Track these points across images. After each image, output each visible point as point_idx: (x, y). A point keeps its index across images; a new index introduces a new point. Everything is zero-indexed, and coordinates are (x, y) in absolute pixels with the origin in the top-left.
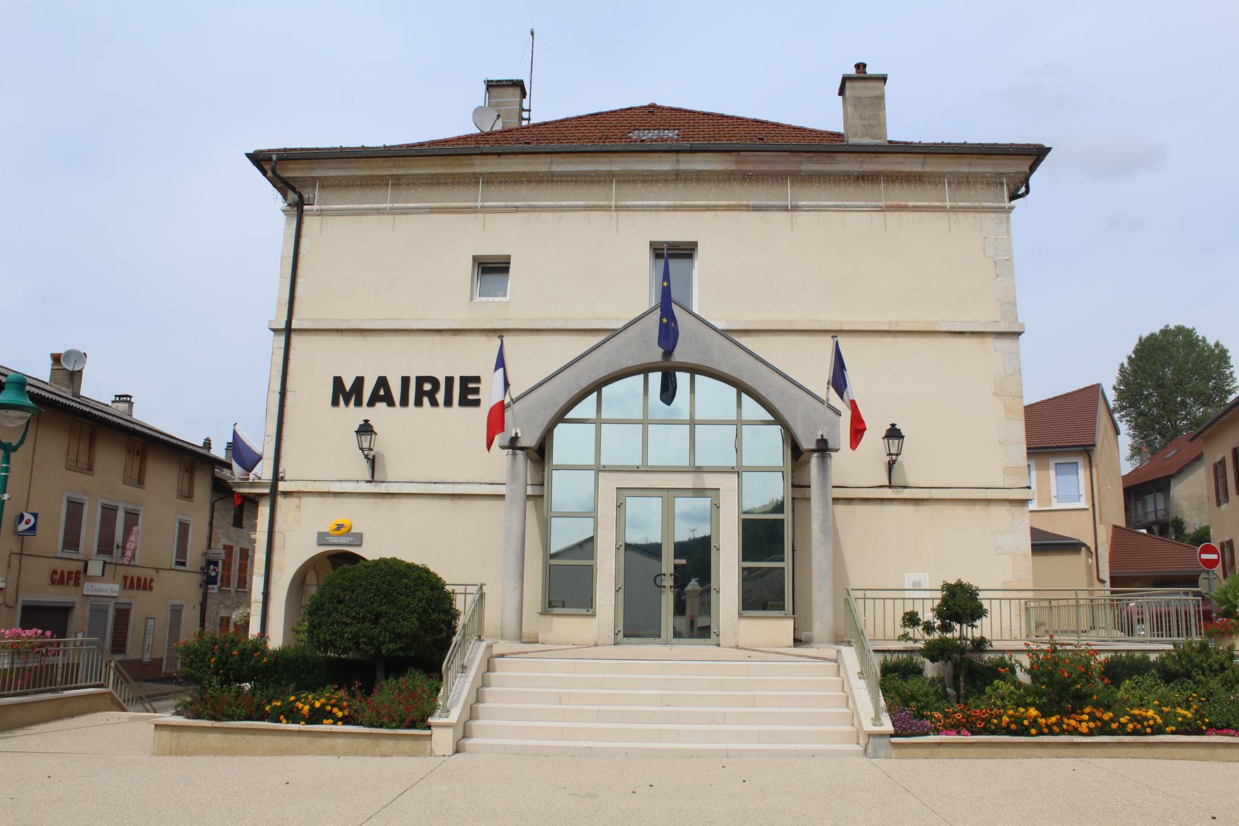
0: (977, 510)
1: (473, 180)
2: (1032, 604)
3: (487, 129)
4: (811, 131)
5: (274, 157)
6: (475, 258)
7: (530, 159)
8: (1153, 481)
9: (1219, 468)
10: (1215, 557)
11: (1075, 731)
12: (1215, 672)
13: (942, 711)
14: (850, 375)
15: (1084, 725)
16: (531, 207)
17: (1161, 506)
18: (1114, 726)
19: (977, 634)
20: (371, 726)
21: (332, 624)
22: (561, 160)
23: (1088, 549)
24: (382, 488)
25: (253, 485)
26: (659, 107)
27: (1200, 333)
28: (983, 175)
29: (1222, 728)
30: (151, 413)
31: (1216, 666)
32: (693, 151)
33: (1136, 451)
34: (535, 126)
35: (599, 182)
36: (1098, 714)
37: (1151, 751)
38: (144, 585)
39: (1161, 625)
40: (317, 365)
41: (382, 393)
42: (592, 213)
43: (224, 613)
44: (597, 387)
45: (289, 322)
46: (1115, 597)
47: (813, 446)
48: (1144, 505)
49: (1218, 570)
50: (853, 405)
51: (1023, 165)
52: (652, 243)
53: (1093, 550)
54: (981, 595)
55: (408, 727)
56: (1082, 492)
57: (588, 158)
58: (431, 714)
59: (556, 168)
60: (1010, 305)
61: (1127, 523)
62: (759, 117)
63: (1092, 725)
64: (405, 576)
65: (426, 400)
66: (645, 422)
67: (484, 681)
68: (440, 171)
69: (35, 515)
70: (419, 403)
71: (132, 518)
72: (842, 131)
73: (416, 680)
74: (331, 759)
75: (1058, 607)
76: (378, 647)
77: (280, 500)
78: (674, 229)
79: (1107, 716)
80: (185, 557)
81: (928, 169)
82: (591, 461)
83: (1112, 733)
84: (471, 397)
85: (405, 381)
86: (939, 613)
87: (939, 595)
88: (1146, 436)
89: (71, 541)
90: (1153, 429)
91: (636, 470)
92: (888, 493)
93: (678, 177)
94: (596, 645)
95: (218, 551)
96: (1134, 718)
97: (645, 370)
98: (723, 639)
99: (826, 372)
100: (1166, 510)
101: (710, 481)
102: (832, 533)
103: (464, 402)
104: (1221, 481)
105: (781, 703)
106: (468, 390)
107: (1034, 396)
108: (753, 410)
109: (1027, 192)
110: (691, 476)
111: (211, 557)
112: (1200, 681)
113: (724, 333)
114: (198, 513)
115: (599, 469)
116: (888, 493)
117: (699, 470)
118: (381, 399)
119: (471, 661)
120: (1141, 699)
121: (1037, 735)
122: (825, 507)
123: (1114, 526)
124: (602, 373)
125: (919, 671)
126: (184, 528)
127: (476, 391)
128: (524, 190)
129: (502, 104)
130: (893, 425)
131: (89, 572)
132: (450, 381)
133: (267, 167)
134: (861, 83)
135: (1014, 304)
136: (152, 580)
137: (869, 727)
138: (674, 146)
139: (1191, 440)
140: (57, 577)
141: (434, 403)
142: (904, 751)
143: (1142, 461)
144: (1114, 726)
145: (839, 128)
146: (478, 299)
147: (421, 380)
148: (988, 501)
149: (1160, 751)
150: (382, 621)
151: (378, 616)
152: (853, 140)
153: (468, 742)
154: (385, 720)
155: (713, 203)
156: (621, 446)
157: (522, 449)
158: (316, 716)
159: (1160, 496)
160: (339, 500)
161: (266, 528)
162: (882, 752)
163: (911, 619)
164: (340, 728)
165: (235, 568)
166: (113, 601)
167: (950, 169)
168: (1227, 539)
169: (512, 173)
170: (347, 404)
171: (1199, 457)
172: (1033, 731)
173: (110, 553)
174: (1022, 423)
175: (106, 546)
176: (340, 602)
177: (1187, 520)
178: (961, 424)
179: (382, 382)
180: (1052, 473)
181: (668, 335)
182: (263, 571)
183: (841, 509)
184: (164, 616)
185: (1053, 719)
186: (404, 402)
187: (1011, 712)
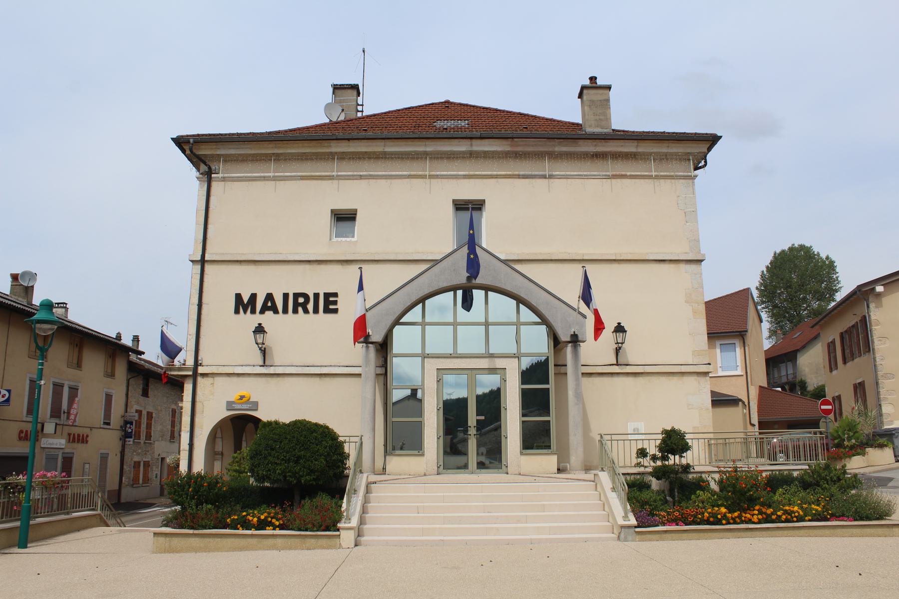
0: (675, 380)
1: (331, 157)
2: (713, 442)
3: (334, 120)
4: (558, 121)
5: (191, 141)
6: (332, 211)
7: (370, 143)
8: (785, 354)
9: (831, 346)
10: (830, 407)
11: (750, 521)
12: (835, 482)
13: (666, 511)
14: (594, 292)
15: (755, 517)
16: (371, 175)
17: (790, 371)
18: (774, 517)
19: (684, 461)
20: (300, 530)
21: (268, 464)
22: (391, 143)
23: (743, 403)
24: (271, 370)
25: (180, 369)
26: (452, 103)
27: (816, 250)
28: (676, 154)
29: (840, 516)
30: (81, 315)
31: (835, 478)
32: (481, 138)
33: (773, 333)
34: (368, 117)
35: (417, 158)
36: (764, 510)
37: (797, 532)
38: (82, 439)
39: (797, 453)
40: (224, 285)
41: (269, 304)
42: (413, 180)
43: (136, 459)
44: (422, 300)
45: (203, 255)
46: (762, 436)
47: (569, 339)
48: (779, 371)
49: (832, 416)
50: (596, 312)
51: (703, 148)
52: (454, 201)
53: (746, 403)
54: (687, 436)
55: (324, 530)
56: (739, 364)
57: (410, 142)
58: (339, 521)
59: (388, 149)
60: (695, 242)
61: (768, 383)
62: (522, 112)
63: (760, 517)
64: (315, 431)
65: (300, 309)
66: (455, 324)
67: (366, 501)
68: (308, 150)
69: (9, 391)
70: (295, 311)
71: (74, 391)
72: (580, 122)
73: (323, 499)
74: (275, 552)
75: (729, 443)
76: (288, 479)
77: (199, 379)
78: (469, 191)
79: (770, 511)
80: (110, 419)
81: (640, 150)
82: (419, 351)
83: (773, 522)
84: (331, 307)
85: (286, 296)
86: (661, 449)
87: (660, 437)
88: (779, 322)
89: (32, 408)
90: (785, 317)
91: (450, 356)
92: (616, 369)
93: (472, 155)
94: (425, 475)
95: (133, 414)
96: (786, 512)
97: (454, 289)
98: (510, 470)
99: (578, 289)
100: (795, 374)
101: (499, 363)
102: (579, 396)
103: (327, 310)
104: (832, 355)
105: (551, 511)
106: (330, 303)
107: (707, 300)
108: (526, 314)
109: (705, 165)
110: (487, 360)
111: (128, 419)
112: (825, 488)
113: (505, 262)
114: (118, 387)
115: (425, 356)
116: (616, 369)
117: (492, 356)
118: (269, 309)
119: (360, 486)
120: (789, 500)
121: (727, 524)
122: (577, 380)
123: (760, 387)
124: (427, 291)
125: (648, 486)
126: (109, 398)
127: (335, 303)
128: (366, 164)
129: (344, 101)
130: (619, 324)
131: (46, 430)
132: (316, 296)
133: (186, 147)
134: (593, 91)
135: (698, 241)
136: (87, 436)
137: (621, 522)
138: (469, 134)
139: (812, 327)
140: (23, 435)
141: (306, 311)
142: (643, 536)
143: (777, 340)
144: (774, 517)
145: (578, 120)
146: (335, 239)
147: (296, 296)
148: (683, 374)
149: (802, 532)
150: (301, 461)
151: (299, 458)
152: (589, 130)
153: (363, 539)
154: (310, 526)
155: (495, 173)
156: (439, 340)
157: (372, 343)
158: (262, 525)
159: (790, 365)
160: (241, 379)
161: (190, 399)
162: (630, 538)
163: (642, 453)
164: (278, 532)
165: (144, 426)
166: (61, 451)
167: (655, 150)
168: (837, 394)
169: (358, 152)
170: (245, 312)
171: (816, 337)
172: (724, 522)
173: (59, 417)
174: (704, 321)
175: (56, 412)
176: (272, 449)
177: (808, 381)
178: (662, 321)
179: (269, 297)
180: (718, 351)
181: (473, 266)
182: (188, 429)
183: (585, 381)
184: (96, 461)
185: (736, 514)
186: (285, 311)
187: (709, 510)
